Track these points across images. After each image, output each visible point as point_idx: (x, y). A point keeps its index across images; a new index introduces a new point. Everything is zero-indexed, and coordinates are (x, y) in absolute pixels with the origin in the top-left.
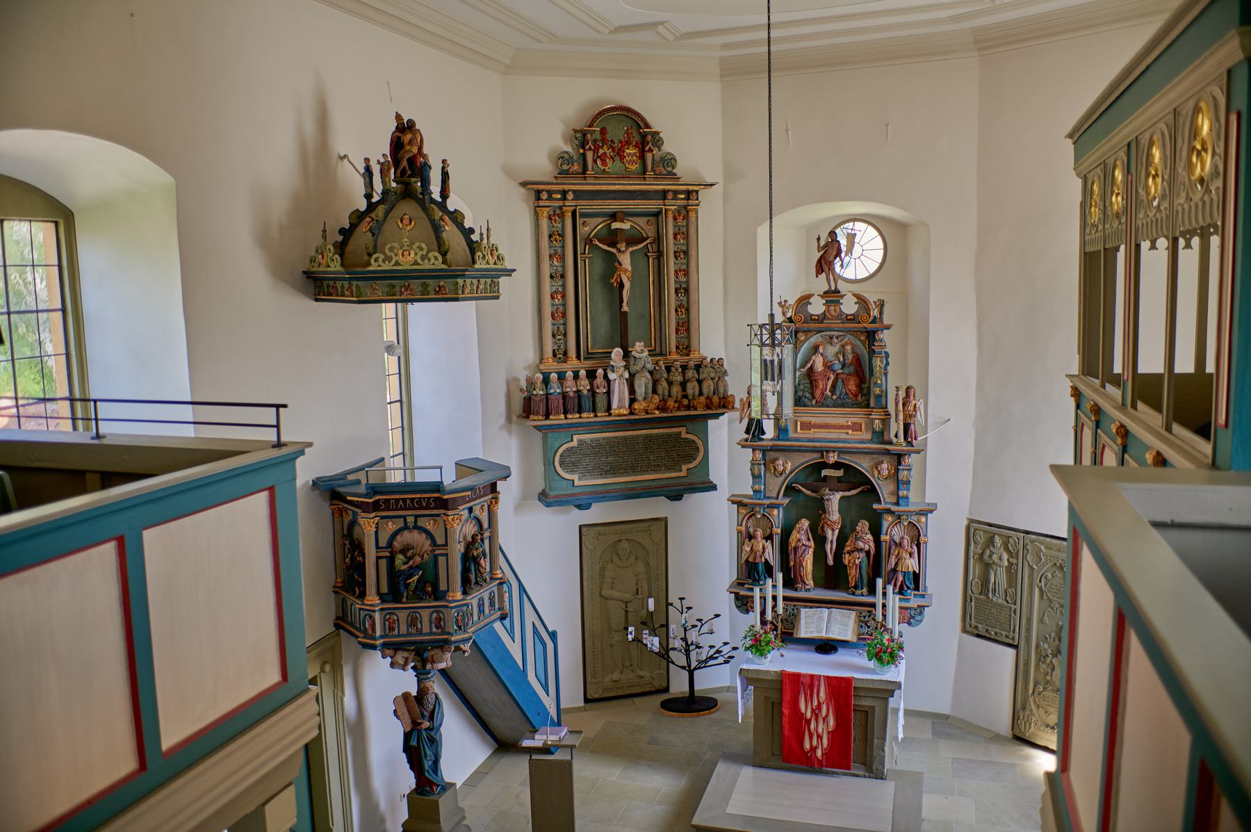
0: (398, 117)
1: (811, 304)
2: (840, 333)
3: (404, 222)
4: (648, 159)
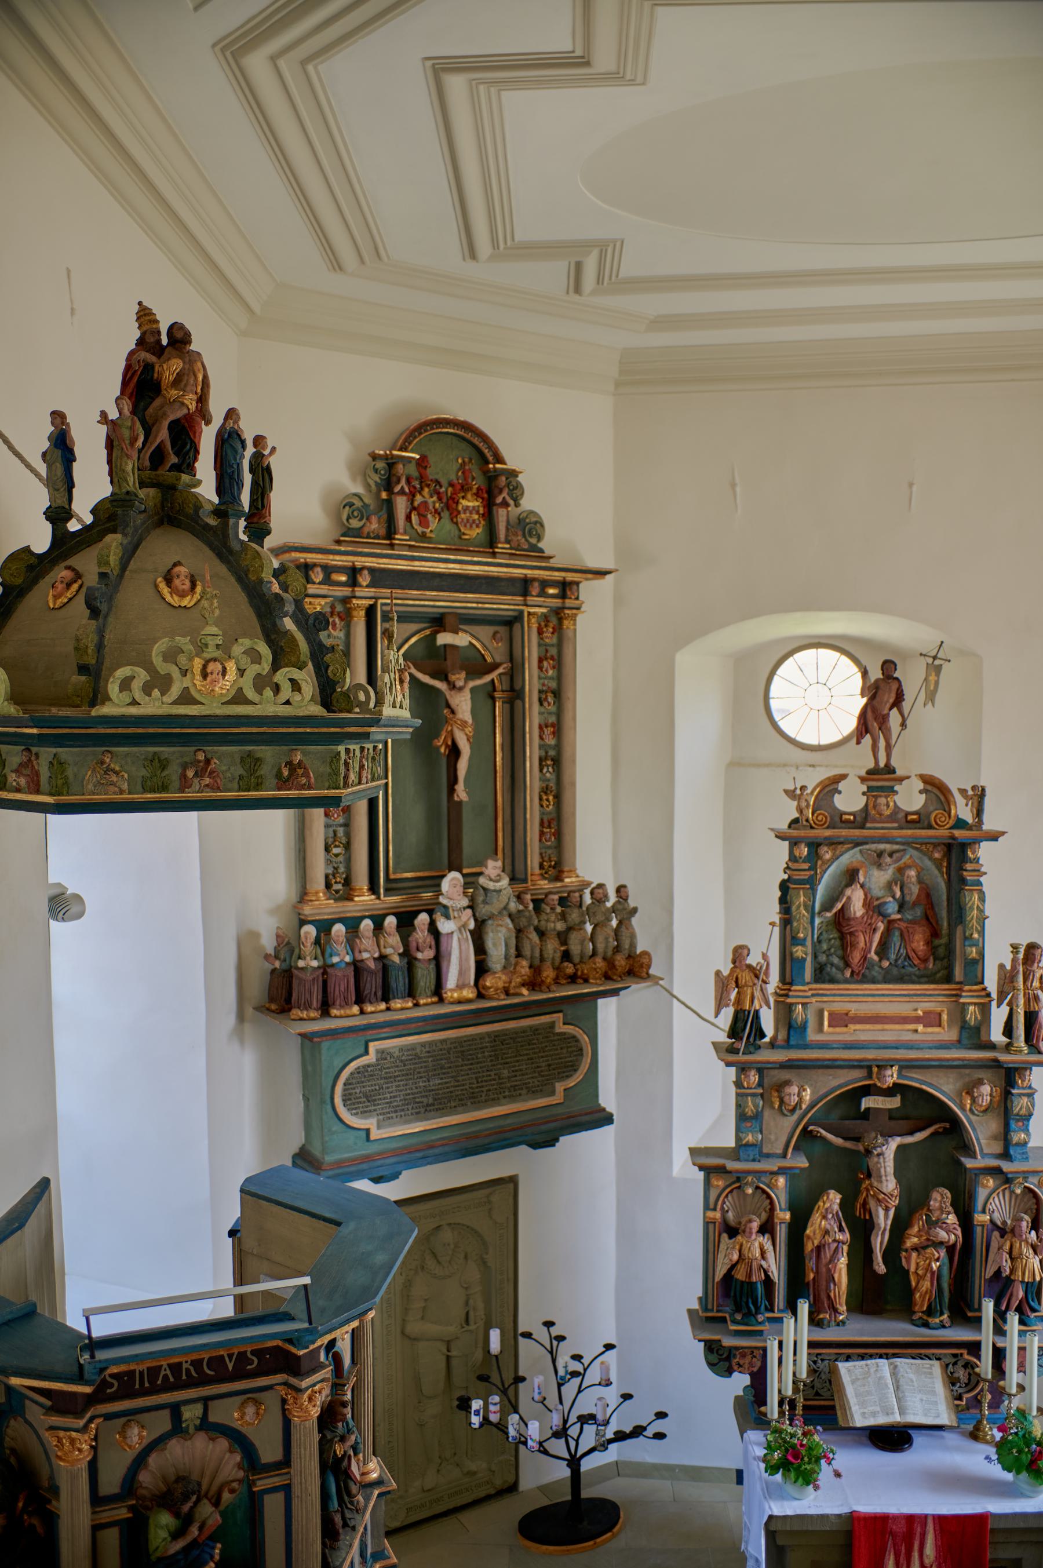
0: (145, 315)
1: (840, 792)
2: (896, 847)
3: (177, 582)
4: (500, 519)
